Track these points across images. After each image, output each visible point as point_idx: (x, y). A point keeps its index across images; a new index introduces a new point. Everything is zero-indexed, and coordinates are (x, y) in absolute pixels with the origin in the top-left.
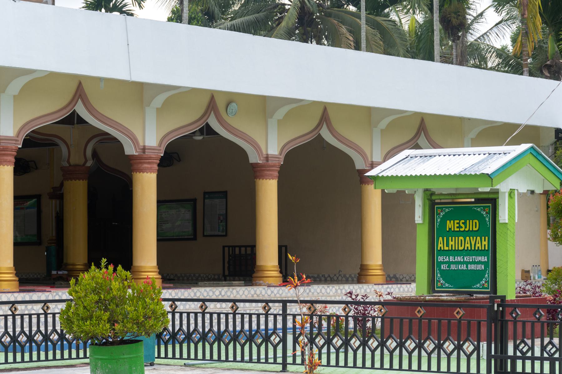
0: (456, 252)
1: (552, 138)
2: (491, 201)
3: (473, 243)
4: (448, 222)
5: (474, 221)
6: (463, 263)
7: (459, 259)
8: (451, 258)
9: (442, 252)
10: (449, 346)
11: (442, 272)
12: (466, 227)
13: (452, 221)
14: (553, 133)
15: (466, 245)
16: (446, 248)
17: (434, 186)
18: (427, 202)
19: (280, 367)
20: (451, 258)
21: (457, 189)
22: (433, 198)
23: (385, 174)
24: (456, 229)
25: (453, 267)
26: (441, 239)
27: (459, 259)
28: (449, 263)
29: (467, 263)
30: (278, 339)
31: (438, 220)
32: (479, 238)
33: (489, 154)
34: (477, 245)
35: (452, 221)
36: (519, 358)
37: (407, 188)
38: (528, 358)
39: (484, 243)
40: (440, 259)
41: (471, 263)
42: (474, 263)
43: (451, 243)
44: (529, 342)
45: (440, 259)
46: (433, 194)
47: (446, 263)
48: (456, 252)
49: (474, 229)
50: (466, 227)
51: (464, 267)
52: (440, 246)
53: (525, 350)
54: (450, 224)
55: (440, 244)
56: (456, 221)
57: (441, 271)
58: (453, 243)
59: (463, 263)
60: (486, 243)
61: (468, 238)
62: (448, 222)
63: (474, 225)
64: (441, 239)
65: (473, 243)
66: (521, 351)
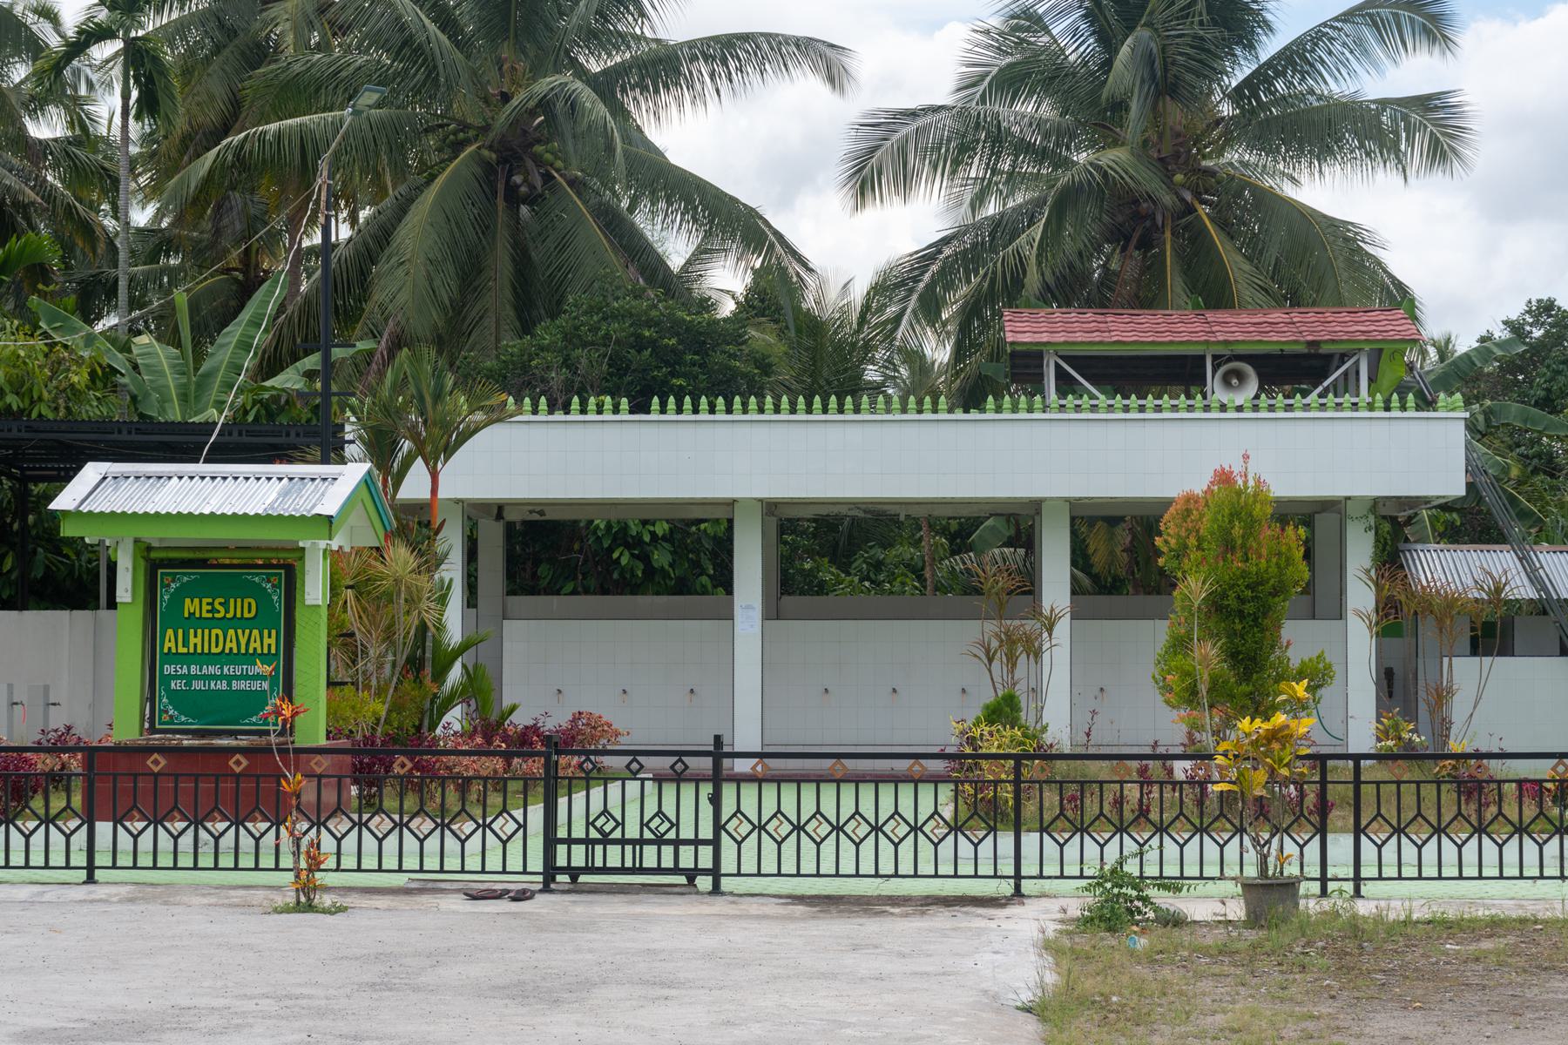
0: (209, 658)
1: (1394, 643)
2: (288, 570)
3: (243, 642)
4: (188, 601)
5: (246, 601)
6: (221, 677)
7: (212, 670)
8: (194, 669)
9: (172, 657)
10: (380, 823)
11: (173, 695)
12: (227, 611)
13: (196, 601)
14: (1386, 640)
15: (228, 645)
16: (182, 650)
17: (151, 534)
18: (142, 563)
19: (83, 874)
20: (194, 669)
21: (161, 540)
22: (153, 555)
23: (99, 505)
24: (205, 615)
25: (197, 685)
26: (170, 632)
27: (212, 670)
28: (189, 678)
29: (229, 679)
30: (512, 826)
31: (163, 598)
32: (255, 632)
33: (291, 479)
34: (252, 645)
35: (196, 601)
36: (650, 842)
37: (108, 535)
38: (668, 842)
39: (266, 641)
40: (169, 669)
41: (237, 678)
42: (246, 677)
43: (192, 640)
44: (518, 814)
45: (169, 669)
46: (149, 548)
47: (182, 677)
48: (209, 658)
49: (246, 615)
50: (227, 611)
51: (223, 685)
52: (167, 645)
53: (607, 828)
54: (190, 606)
55: (169, 642)
56: (205, 601)
57: (173, 695)
58: (198, 640)
59: (221, 677)
60: (273, 641)
61: (231, 632)
62: (188, 601)
63: (246, 607)
64: (170, 632)
65: (243, 642)
66: (600, 830)
